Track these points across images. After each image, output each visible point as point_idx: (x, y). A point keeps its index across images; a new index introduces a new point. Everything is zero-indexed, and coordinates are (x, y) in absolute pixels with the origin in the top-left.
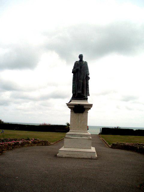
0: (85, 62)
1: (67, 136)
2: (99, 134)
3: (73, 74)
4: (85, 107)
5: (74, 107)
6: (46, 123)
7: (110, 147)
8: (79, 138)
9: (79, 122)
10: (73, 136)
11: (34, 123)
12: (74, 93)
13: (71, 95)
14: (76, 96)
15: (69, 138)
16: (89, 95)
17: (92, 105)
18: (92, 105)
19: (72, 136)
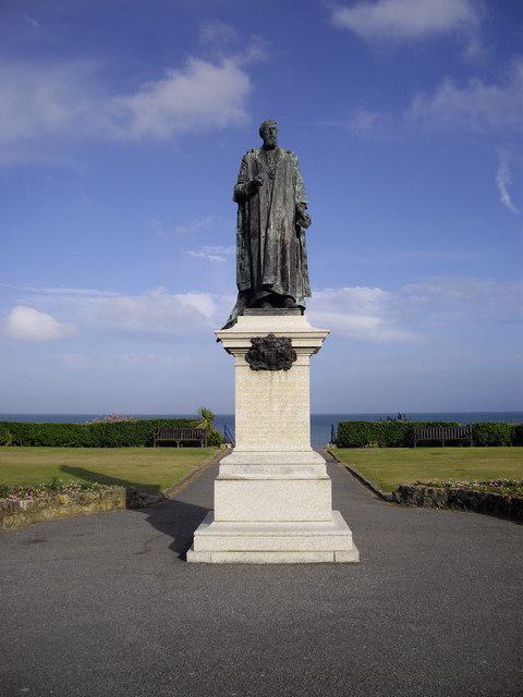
1: (223, 470)
4: (294, 344)
9: (276, 408)
15: (242, 479)
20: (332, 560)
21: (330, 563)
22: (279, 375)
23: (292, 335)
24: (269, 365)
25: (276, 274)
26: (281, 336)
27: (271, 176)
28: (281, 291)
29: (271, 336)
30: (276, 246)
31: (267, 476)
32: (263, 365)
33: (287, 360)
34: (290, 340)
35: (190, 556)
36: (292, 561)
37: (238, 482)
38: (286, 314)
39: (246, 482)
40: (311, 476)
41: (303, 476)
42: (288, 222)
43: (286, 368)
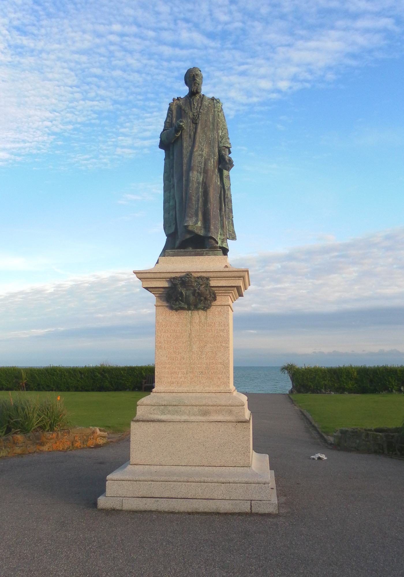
0: (213, 99)
1: (141, 412)
2: (291, 392)
3: (163, 151)
4: (213, 283)
5: (166, 285)
6: (371, 366)
7: (331, 444)
8: (192, 418)
9: (195, 348)
10: (169, 412)
11: (29, 366)
12: (173, 230)
13: (163, 239)
14: (178, 243)
15: (153, 421)
16: (234, 238)
17: (243, 296)
18: (243, 296)
19: (163, 413)
20: (248, 510)
21: (246, 514)
22: (198, 316)
23: (211, 275)
24: (189, 304)
25: (197, 216)
26: (199, 275)
27: (195, 121)
28: (202, 233)
29: (188, 274)
30: (198, 188)
31: (184, 418)
32: (183, 305)
33: (292, 368)
34: (208, 279)
35: (103, 502)
36: (182, 509)
37: (152, 424)
38: (207, 254)
39: (162, 424)
40: (228, 418)
41: (220, 418)
42: (212, 163)
43: (206, 308)
